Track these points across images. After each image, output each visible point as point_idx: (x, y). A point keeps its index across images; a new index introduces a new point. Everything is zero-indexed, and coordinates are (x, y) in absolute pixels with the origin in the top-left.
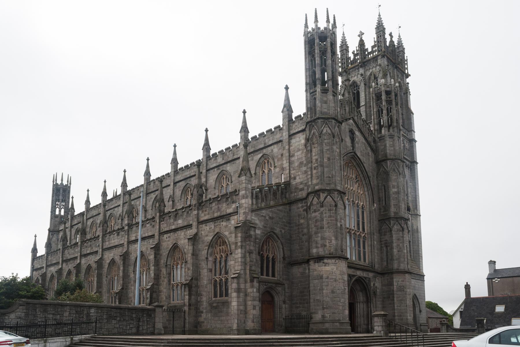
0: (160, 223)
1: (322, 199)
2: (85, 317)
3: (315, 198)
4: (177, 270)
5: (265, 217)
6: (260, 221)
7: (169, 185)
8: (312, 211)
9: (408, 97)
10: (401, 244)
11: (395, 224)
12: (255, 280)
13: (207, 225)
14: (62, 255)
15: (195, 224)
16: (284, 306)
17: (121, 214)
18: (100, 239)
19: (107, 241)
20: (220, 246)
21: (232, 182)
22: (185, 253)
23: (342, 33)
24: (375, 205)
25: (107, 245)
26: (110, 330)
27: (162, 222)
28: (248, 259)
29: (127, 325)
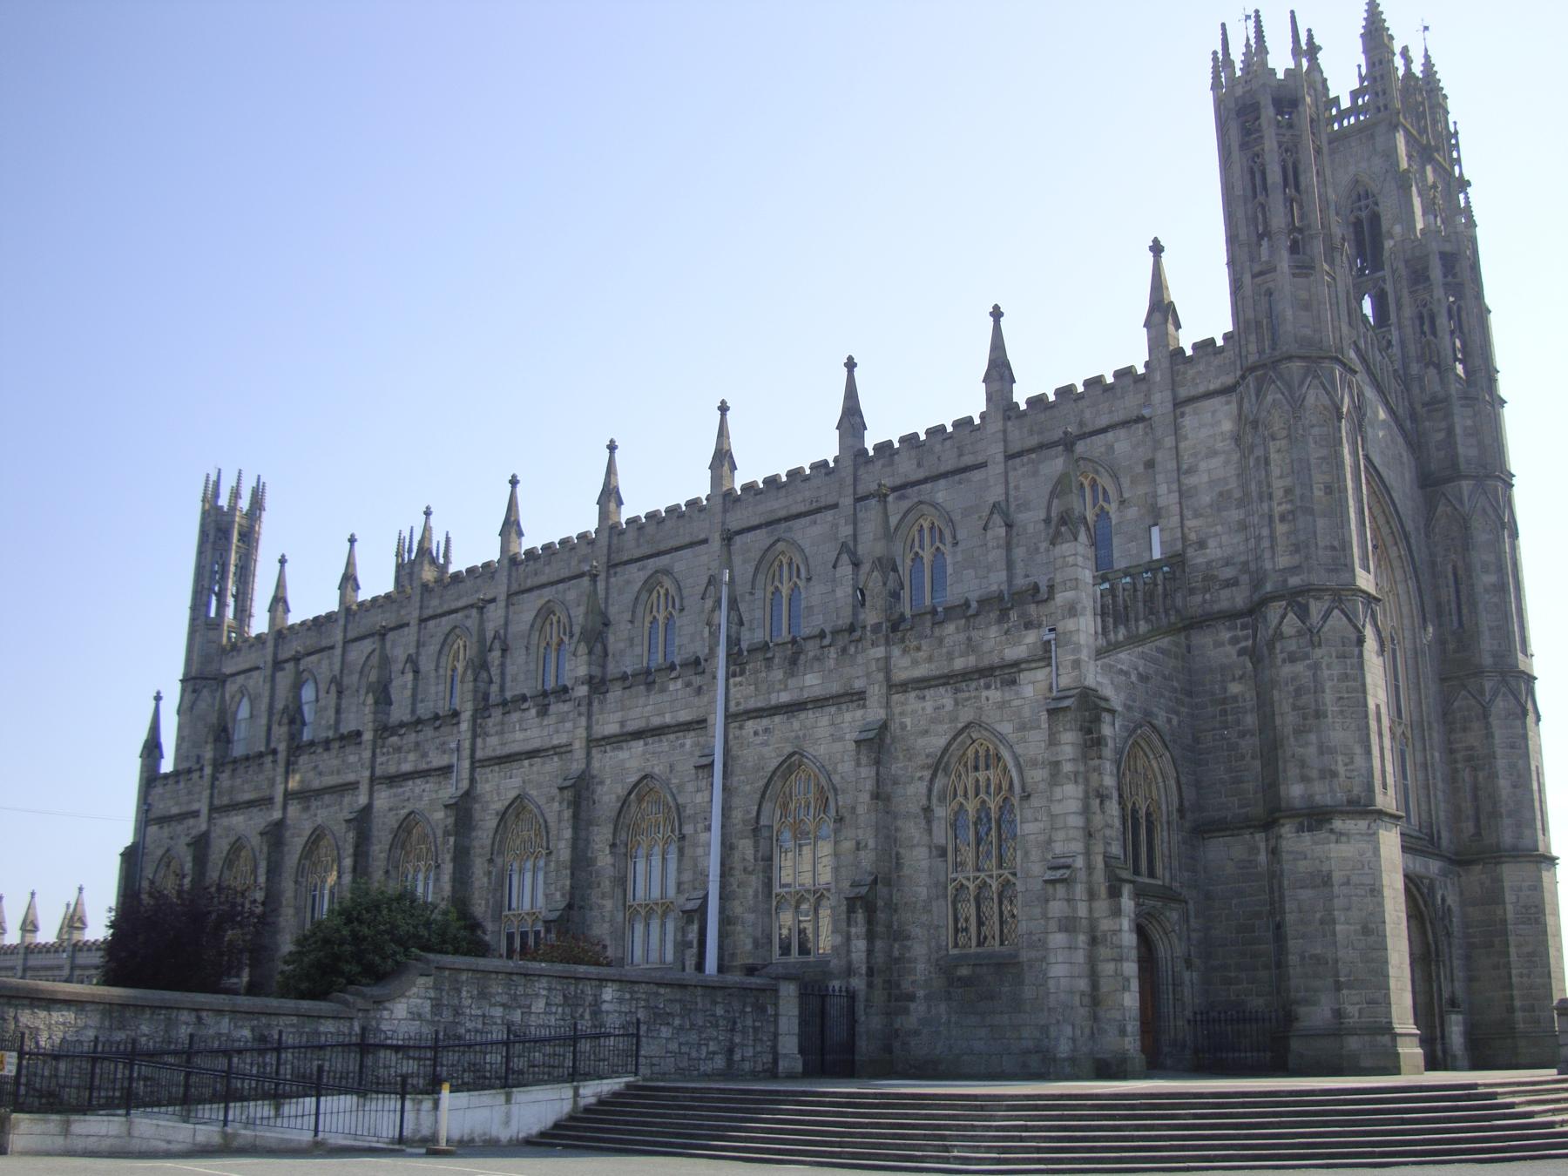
2: (587, 1016)
3: (1291, 615)
5: (1126, 674)
6: (1117, 688)
8: (1280, 657)
10: (1520, 762)
11: (1495, 694)
13: (924, 698)
16: (1187, 975)
17: (502, 632)
18: (464, 726)
19: (492, 731)
20: (976, 768)
22: (835, 790)
25: (492, 745)
26: (655, 1061)
29: (700, 1045)
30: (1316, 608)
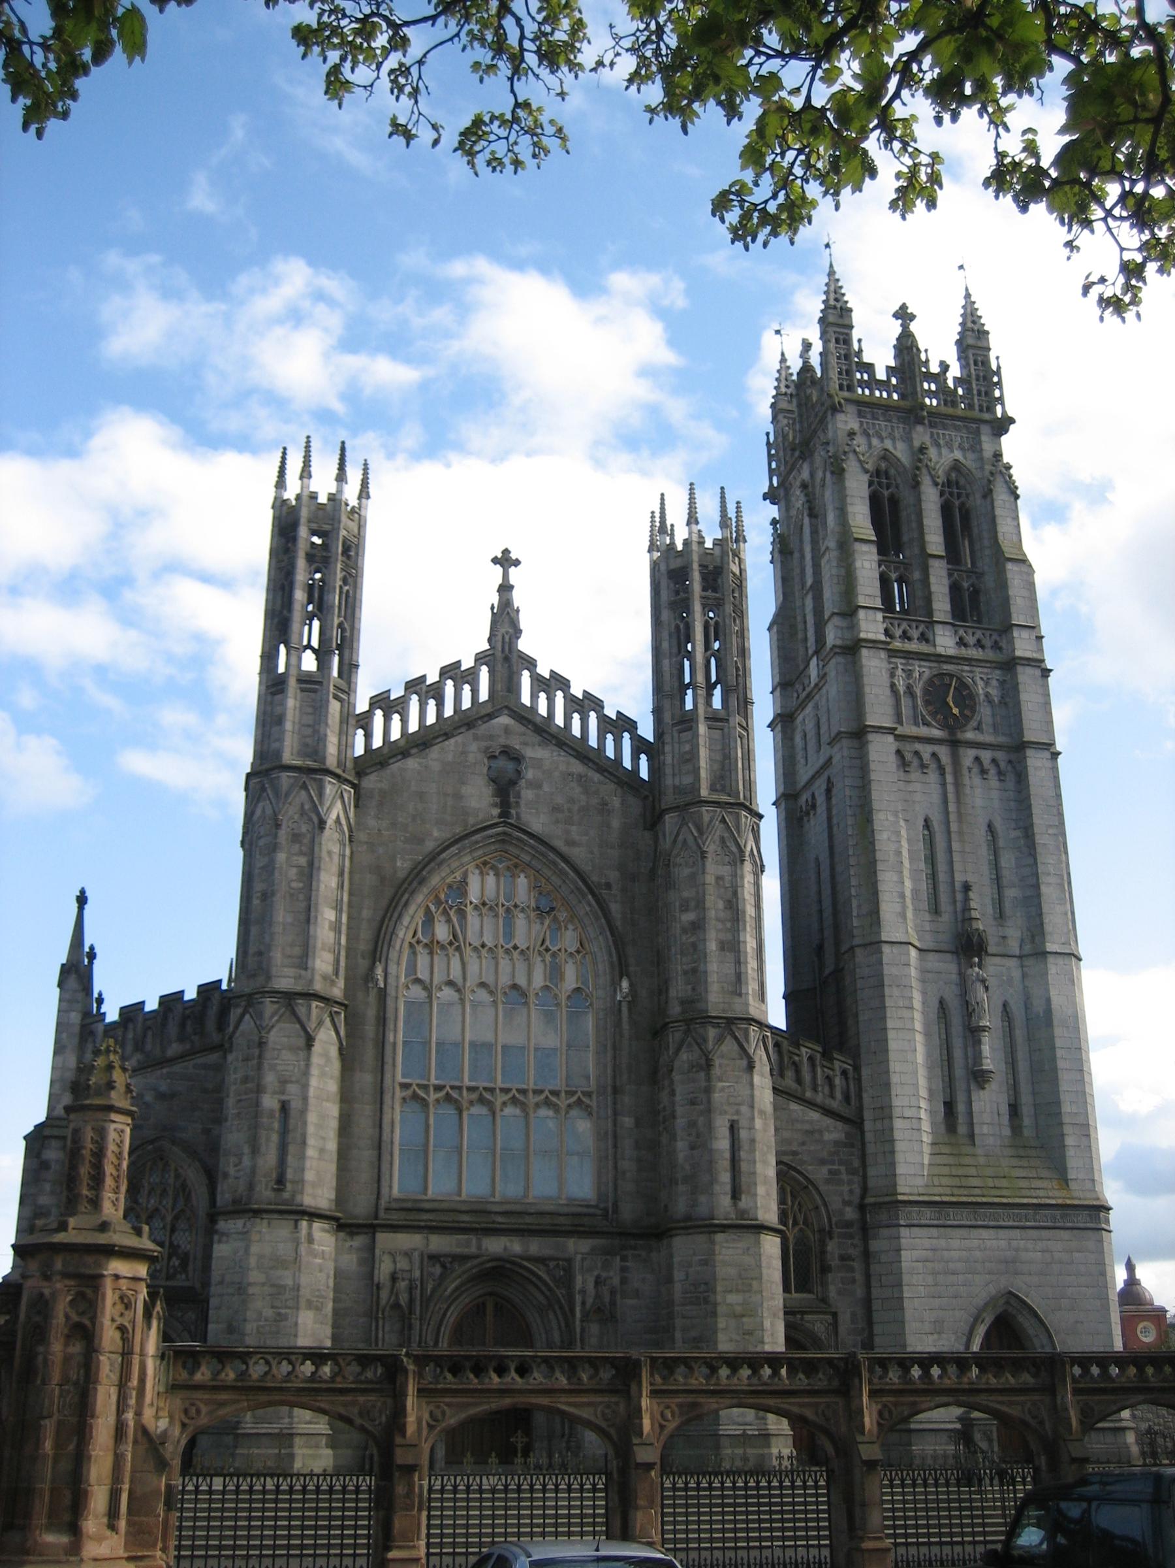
23: (964, 293)
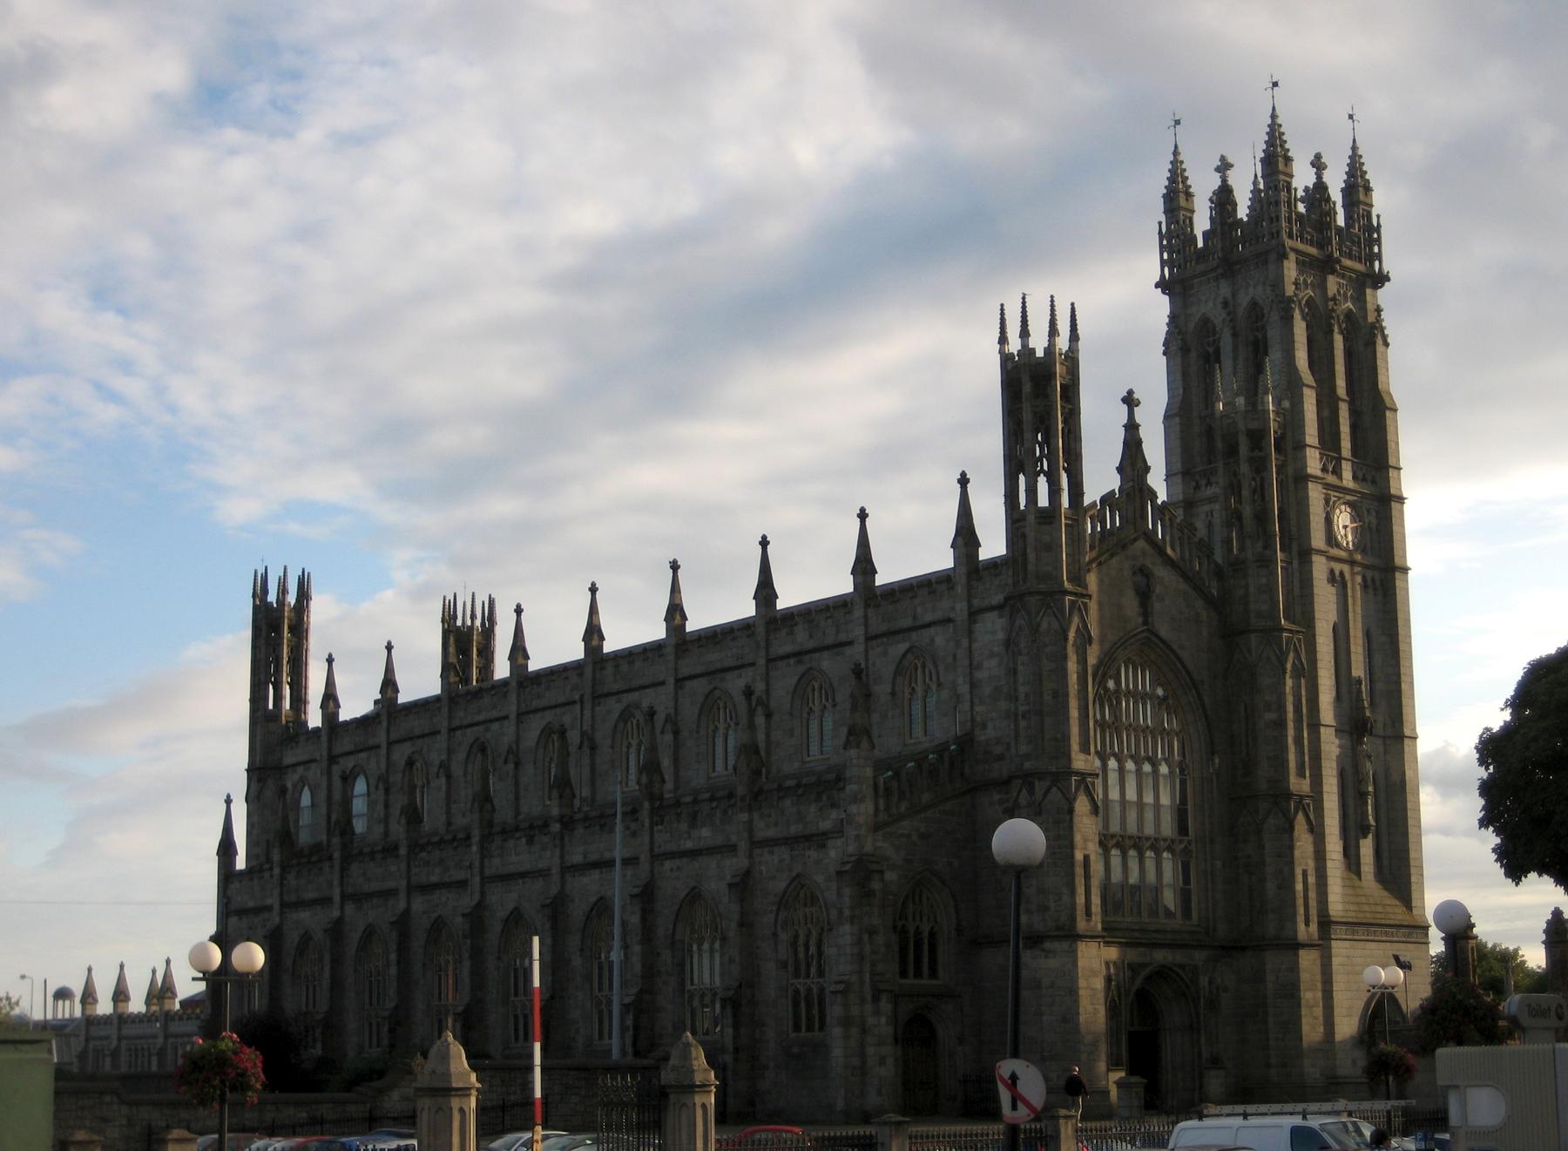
0: (652, 828)
1: (1039, 794)
3: (1024, 790)
4: (700, 956)
7: (662, 683)
9: (1379, 355)
12: (884, 998)
13: (773, 852)
14: (342, 877)
15: (743, 846)
17: (514, 747)
18: (474, 848)
20: (805, 905)
21: (834, 706)
24: (1217, 761)
25: (495, 865)
27: (657, 824)
28: (867, 949)
30: (1040, 787)
